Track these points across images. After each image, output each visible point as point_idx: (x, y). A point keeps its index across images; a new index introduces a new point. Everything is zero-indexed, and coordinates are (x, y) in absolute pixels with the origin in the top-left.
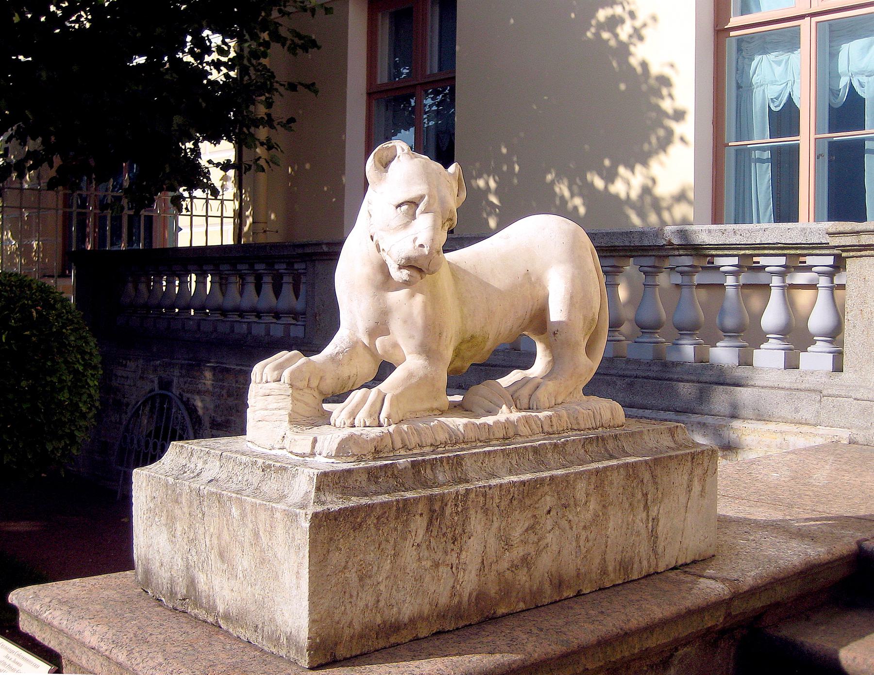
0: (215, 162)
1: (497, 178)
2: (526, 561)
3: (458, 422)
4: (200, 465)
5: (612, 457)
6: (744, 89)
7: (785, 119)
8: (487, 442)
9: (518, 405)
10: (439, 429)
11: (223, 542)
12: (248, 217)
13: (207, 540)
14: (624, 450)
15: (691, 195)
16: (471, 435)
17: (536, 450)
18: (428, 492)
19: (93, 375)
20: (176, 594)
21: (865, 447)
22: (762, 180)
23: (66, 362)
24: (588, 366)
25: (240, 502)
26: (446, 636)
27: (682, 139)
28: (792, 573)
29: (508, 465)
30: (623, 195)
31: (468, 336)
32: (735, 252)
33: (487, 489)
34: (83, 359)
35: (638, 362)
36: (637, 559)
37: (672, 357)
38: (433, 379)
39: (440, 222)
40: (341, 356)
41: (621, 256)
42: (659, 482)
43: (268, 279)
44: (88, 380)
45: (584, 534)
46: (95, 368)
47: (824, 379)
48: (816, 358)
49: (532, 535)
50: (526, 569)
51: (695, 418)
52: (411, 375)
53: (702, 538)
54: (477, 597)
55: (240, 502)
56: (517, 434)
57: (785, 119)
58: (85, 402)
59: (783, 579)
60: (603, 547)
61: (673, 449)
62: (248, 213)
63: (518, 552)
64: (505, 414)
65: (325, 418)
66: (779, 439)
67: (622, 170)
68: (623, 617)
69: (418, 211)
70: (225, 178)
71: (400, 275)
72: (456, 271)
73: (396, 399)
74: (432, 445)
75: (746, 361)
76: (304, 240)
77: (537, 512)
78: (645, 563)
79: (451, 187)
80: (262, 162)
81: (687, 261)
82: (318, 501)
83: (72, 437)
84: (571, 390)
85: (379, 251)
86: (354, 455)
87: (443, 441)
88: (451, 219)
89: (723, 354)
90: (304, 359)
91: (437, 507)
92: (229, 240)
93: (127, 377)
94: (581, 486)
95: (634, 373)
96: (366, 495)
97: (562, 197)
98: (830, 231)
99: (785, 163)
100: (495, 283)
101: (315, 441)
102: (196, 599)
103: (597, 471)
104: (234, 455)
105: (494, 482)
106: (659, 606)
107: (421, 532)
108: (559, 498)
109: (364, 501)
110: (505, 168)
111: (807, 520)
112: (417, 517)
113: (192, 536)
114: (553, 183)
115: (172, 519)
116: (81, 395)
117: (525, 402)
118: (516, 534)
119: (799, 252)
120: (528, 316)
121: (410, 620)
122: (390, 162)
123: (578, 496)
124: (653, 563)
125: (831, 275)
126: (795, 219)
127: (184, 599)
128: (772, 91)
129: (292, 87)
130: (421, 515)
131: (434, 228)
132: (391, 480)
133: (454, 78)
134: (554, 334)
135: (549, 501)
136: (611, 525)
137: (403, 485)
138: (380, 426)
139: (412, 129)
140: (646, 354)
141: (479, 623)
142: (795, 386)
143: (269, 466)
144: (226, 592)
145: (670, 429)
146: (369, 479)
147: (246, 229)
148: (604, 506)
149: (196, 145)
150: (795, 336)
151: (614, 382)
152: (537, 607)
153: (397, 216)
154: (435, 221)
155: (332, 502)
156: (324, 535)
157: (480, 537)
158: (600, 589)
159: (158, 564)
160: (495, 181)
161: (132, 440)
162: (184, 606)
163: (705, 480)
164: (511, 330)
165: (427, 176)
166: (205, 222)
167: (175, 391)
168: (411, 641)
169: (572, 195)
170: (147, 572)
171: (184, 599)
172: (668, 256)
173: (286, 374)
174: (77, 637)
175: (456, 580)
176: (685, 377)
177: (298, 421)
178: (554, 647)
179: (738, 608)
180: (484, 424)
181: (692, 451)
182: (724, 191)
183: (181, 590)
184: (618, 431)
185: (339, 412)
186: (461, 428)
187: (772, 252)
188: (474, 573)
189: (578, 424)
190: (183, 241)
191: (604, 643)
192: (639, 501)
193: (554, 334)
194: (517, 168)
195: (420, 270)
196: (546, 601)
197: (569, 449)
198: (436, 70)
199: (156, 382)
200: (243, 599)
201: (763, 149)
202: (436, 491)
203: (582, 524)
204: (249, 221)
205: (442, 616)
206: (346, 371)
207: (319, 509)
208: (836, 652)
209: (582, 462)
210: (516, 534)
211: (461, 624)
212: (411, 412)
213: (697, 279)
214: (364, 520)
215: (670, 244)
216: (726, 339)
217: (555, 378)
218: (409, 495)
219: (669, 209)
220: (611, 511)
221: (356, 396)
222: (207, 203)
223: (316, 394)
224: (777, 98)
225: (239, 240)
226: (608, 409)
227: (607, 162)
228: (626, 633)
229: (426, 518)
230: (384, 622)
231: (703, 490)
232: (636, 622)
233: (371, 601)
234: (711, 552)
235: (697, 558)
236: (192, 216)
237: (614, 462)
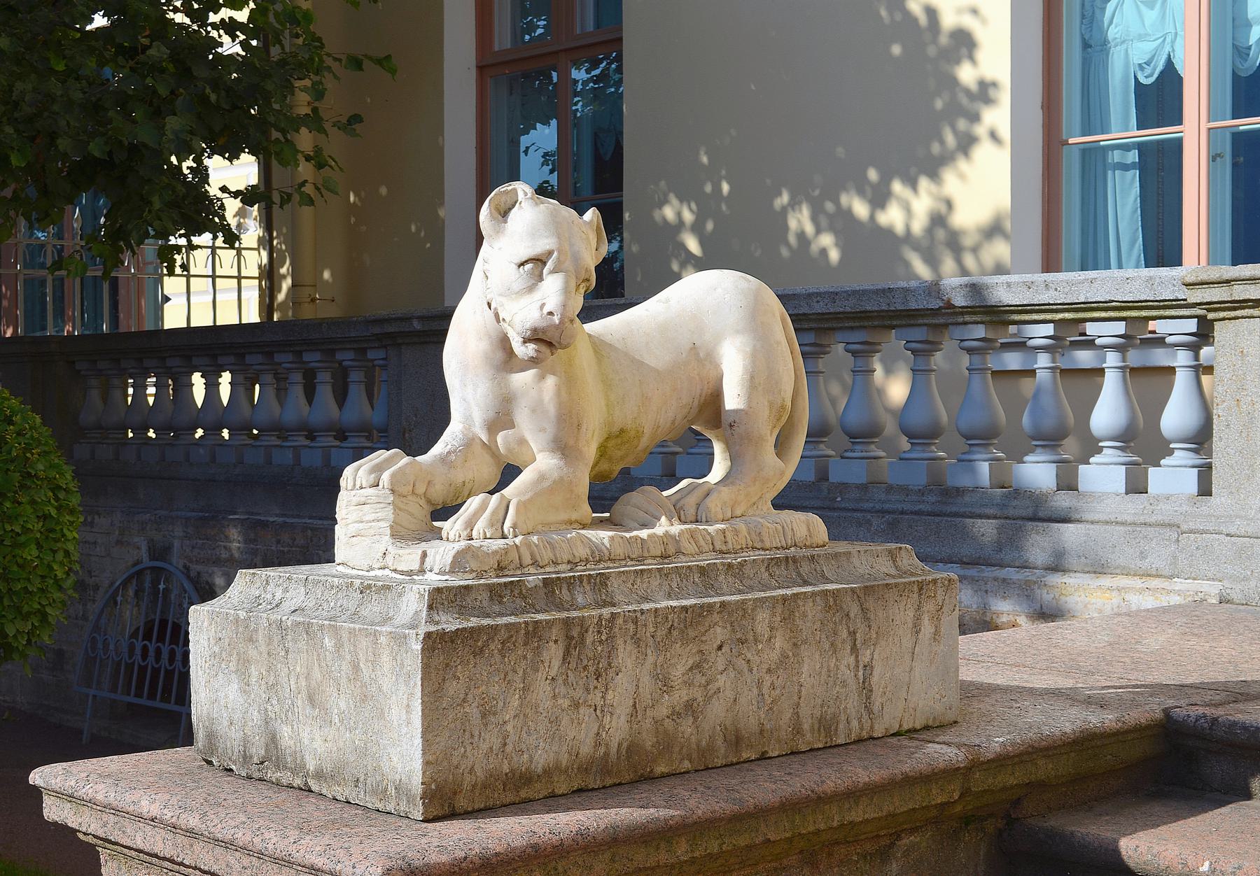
0: (233, 189)
1: (693, 206)
2: (689, 706)
3: (603, 536)
4: (279, 595)
5: (806, 583)
6: (1095, 48)
7: (1160, 97)
8: (641, 560)
9: (683, 518)
10: (579, 543)
11: (313, 683)
12: (284, 277)
13: (292, 683)
14: (823, 576)
15: (1008, 225)
16: (619, 551)
17: (703, 571)
18: (565, 615)
19: (72, 523)
20: (251, 757)
21: (1242, 607)
22: (1124, 197)
23: (33, 502)
24: (781, 470)
25: (335, 629)
26: (590, 794)
27: (993, 136)
28: (1060, 743)
29: (667, 588)
30: (899, 228)
31: (615, 429)
32: (1049, 316)
33: (639, 614)
34: (57, 499)
35: (904, 490)
36: (843, 717)
37: (964, 481)
38: (571, 482)
39: (573, 284)
40: (453, 457)
41: (875, 327)
42: (872, 617)
43: (324, 377)
44: (65, 531)
45: (768, 680)
46: (72, 512)
47: (1185, 508)
48: (1173, 477)
49: (699, 676)
50: (691, 719)
51: (989, 572)
52: (542, 477)
53: (938, 696)
54: (628, 748)
55: (335, 629)
56: (679, 552)
57: (1160, 97)
58: (62, 563)
59: (1047, 749)
60: (796, 698)
61: (894, 577)
62: (283, 270)
63: (681, 696)
64: (664, 527)
65: (437, 535)
66: (1115, 599)
67: (897, 187)
68: (816, 778)
69: (545, 271)
70: (241, 214)
71: (523, 351)
72: (598, 345)
73: (523, 506)
74: (569, 562)
75: (1068, 483)
76: (383, 313)
77: (704, 647)
78: (855, 724)
79: (588, 238)
80: (308, 189)
81: (980, 331)
82: (430, 620)
83: (44, 616)
84: (754, 500)
85: (498, 321)
86: (472, 571)
87: (583, 557)
88: (588, 280)
89: (1037, 472)
90: (407, 459)
91: (575, 633)
92: (252, 315)
93: (95, 543)
94: (763, 616)
95: (900, 507)
96: (488, 616)
97: (801, 236)
98: (1189, 279)
99: (1161, 166)
100: (651, 361)
101: (424, 555)
102: (278, 758)
103: (785, 599)
104: (323, 578)
105: (646, 606)
106: (865, 768)
107: (556, 663)
108: (734, 631)
109: (486, 622)
110: (708, 188)
111: (1103, 688)
112: (551, 644)
113: (272, 680)
114: (784, 210)
115: (244, 664)
116: (54, 552)
117: (691, 512)
118: (678, 672)
119: (1144, 313)
120: (696, 402)
121: (545, 771)
122: (510, 209)
123: (759, 630)
124: (867, 726)
125: (1194, 348)
126: (1179, 263)
127: (262, 763)
128: (1140, 51)
129: (356, 63)
130: (556, 641)
131: (566, 291)
132: (518, 601)
133: (620, 39)
134: (731, 426)
135: (720, 633)
136: (805, 668)
137: (533, 606)
138: (504, 537)
139: (554, 122)
140: (918, 478)
141: (631, 783)
142: (1142, 519)
143: (369, 586)
144: (318, 744)
145: (890, 551)
146: (491, 599)
147: (281, 297)
148: (795, 644)
149: (198, 160)
150: (1143, 444)
151: (869, 522)
152: (708, 769)
153: (516, 278)
154: (567, 283)
155: (447, 622)
156: (439, 659)
157: (631, 674)
158: (792, 753)
159: (226, 723)
160: (691, 210)
161: (106, 646)
162: (266, 771)
163: (939, 619)
164: (673, 422)
165: (557, 227)
166: (211, 288)
167: (177, 561)
168: (545, 797)
169: (818, 231)
170: (211, 736)
171: (262, 763)
172: (946, 325)
173: (386, 477)
174: (131, 809)
175: (601, 726)
176: (978, 511)
177: (400, 534)
178: (723, 805)
179: (980, 782)
180: (636, 538)
181: (919, 579)
182: (1061, 216)
183: (258, 751)
184: (817, 551)
185: (452, 527)
186: (606, 541)
187: (1103, 314)
188: (623, 718)
189: (762, 541)
190: (173, 318)
191: (791, 807)
192: (844, 641)
193: (731, 426)
194: (725, 187)
195: (550, 344)
196: (719, 762)
197: (748, 571)
198: (590, 26)
199: (144, 548)
200: (339, 749)
201: (1126, 148)
202: (574, 614)
203: (765, 666)
204: (286, 284)
205: (585, 769)
206: (459, 476)
207: (433, 628)
208: (1116, 841)
209: (766, 587)
210: (678, 672)
211: (609, 782)
212: (544, 525)
213: (993, 362)
214: (486, 645)
215: (949, 305)
216: (1039, 450)
217: (733, 483)
218: (540, 617)
219: (975, 250)
220: (805, 651)
221: (473, 503)
222: (214, 254)
223: (423, 502)
224: (1148, 63)
225: (270, 316)
226: (807, 526)
227: (873, 175)
228: (819, 798)
229: (561, 645)
230: (512, 771)
231: (937, 632)
232: (832, 784)
233: (496, 742)
234: (951, 716)
235: (930, 723)
236: (188, 277)
237: (809, 589)
